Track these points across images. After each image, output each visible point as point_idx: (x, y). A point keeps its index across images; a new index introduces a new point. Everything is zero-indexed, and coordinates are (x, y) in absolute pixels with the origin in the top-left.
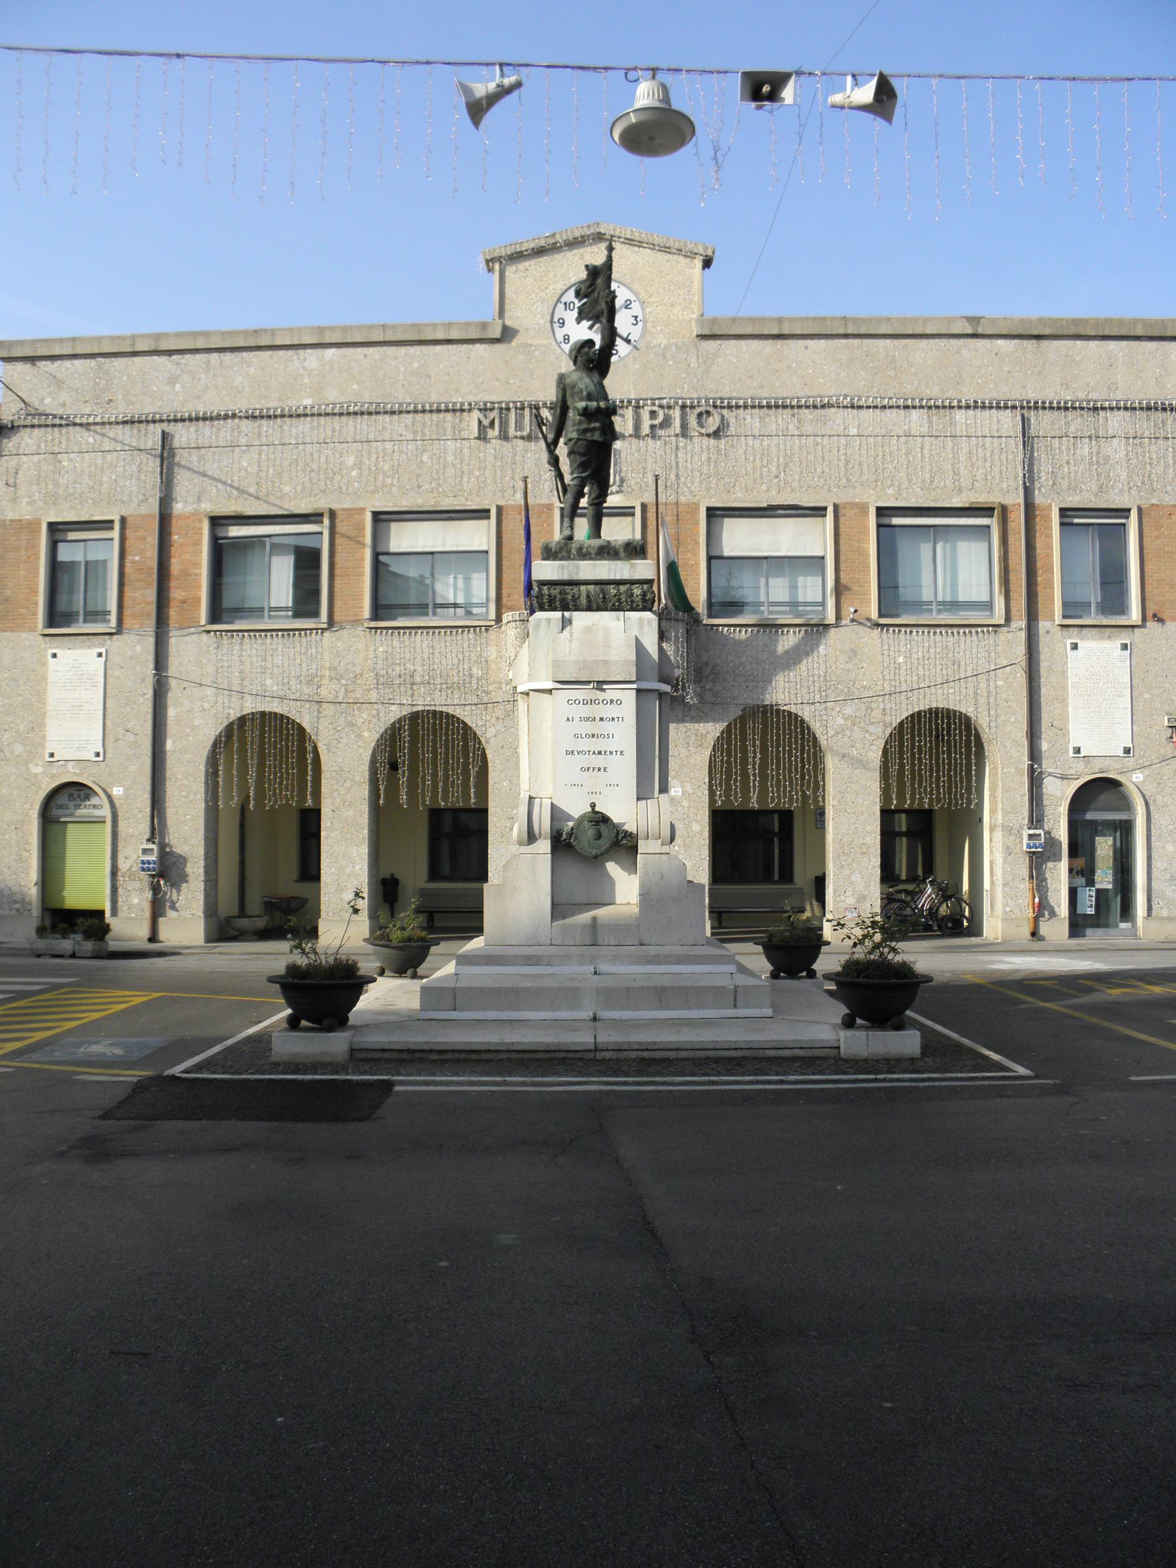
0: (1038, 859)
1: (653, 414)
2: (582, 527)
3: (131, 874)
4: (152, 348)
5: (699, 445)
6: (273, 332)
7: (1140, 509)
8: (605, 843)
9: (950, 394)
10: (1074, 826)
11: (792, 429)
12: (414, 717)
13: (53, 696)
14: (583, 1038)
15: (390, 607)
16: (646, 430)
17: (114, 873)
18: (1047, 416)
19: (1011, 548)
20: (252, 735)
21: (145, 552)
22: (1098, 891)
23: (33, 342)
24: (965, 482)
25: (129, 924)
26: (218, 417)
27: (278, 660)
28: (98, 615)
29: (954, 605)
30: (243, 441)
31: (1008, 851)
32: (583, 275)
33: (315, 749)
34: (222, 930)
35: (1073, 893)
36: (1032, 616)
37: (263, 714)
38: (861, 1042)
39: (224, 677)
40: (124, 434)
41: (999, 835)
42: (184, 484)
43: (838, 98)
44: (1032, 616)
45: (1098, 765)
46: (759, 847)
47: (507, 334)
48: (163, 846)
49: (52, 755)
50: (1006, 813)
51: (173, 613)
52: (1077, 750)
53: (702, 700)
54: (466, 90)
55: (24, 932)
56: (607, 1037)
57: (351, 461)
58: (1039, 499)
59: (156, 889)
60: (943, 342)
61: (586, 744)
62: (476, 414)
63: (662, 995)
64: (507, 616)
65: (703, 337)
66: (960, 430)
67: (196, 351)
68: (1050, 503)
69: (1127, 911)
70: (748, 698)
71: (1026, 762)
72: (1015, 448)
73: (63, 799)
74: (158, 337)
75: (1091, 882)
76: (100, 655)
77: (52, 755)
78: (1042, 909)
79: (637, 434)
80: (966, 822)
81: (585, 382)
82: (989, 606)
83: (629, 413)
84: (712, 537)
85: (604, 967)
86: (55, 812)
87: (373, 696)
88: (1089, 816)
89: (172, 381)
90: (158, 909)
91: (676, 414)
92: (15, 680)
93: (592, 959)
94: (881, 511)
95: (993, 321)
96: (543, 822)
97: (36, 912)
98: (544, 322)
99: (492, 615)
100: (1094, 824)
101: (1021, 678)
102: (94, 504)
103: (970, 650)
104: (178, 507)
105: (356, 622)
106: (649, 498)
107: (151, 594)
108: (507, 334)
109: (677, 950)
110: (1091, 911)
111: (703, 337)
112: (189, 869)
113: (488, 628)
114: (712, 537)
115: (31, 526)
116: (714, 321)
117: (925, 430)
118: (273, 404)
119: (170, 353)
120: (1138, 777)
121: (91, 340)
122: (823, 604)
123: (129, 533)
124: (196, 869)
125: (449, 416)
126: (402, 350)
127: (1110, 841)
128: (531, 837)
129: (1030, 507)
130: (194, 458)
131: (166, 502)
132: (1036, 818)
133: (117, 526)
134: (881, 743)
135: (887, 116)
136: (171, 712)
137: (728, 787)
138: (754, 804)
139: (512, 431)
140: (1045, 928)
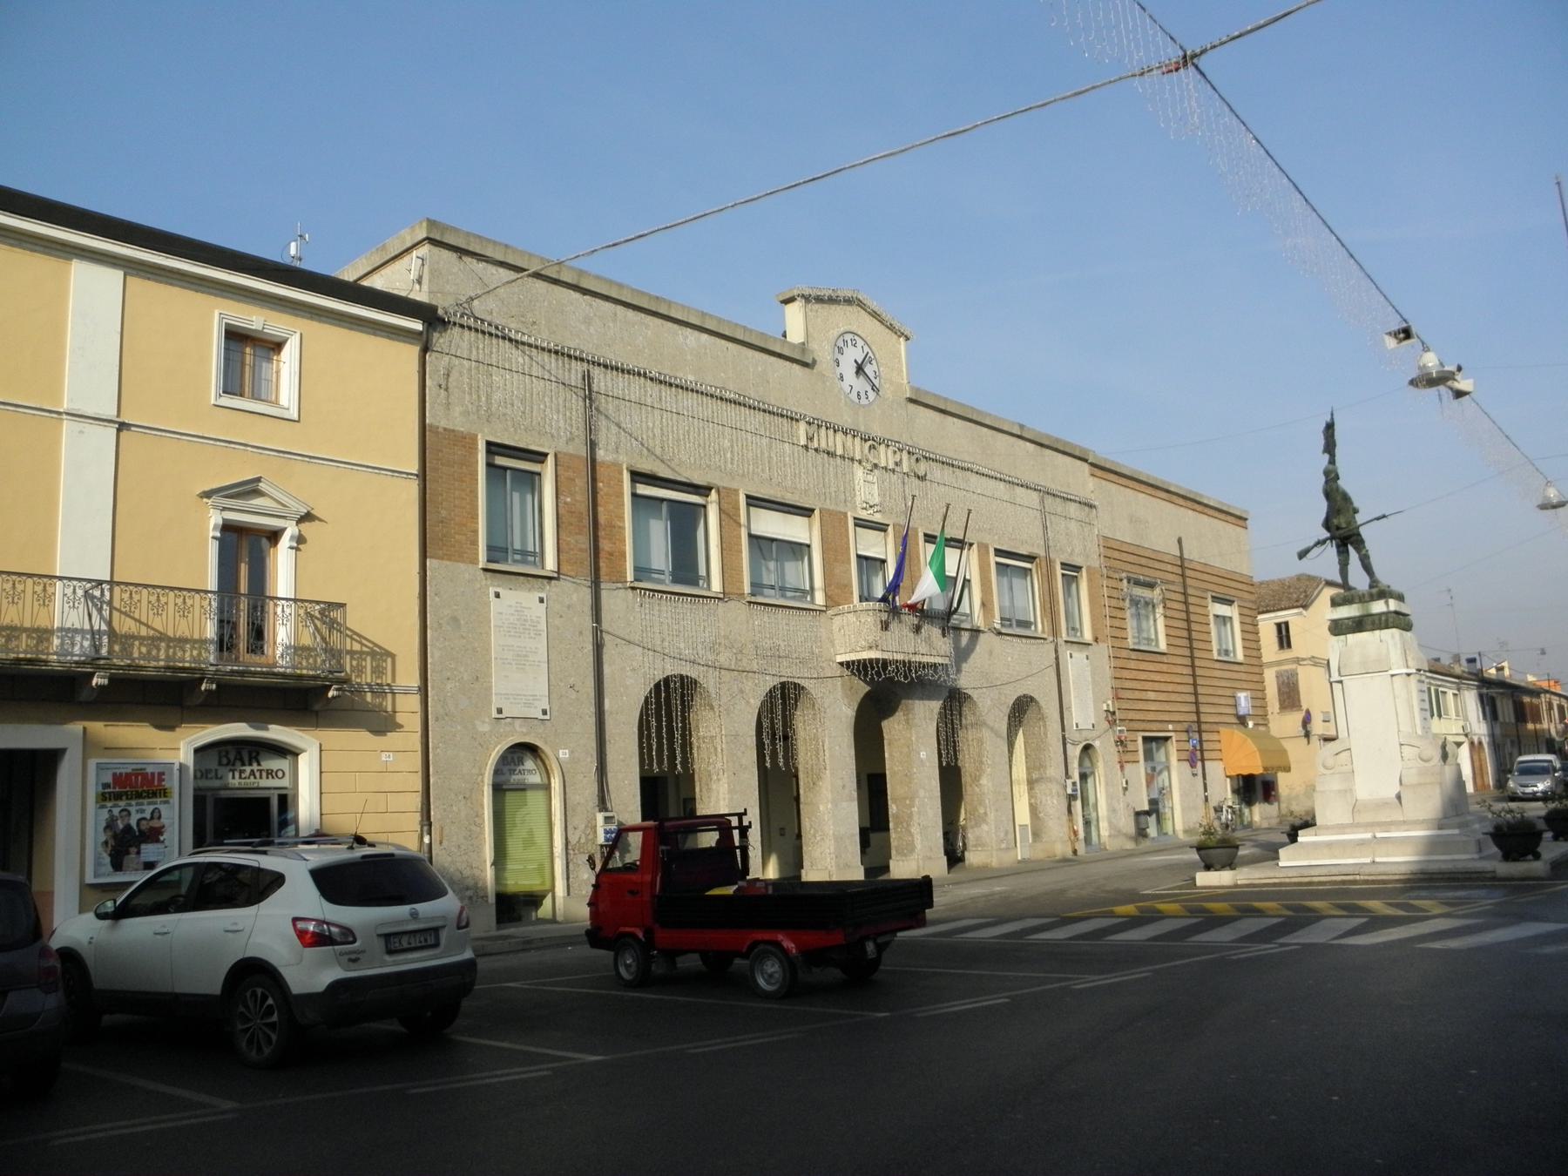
4: (574, 282)
6: (670, 303)
23: (468, 234)
40: (551, 362)
65: (911, 400)
76: (497, 595)
92: (455, 620)
97: (492, 899)
111: (911, 400)
116: (918, 390)
119: (585, 292)
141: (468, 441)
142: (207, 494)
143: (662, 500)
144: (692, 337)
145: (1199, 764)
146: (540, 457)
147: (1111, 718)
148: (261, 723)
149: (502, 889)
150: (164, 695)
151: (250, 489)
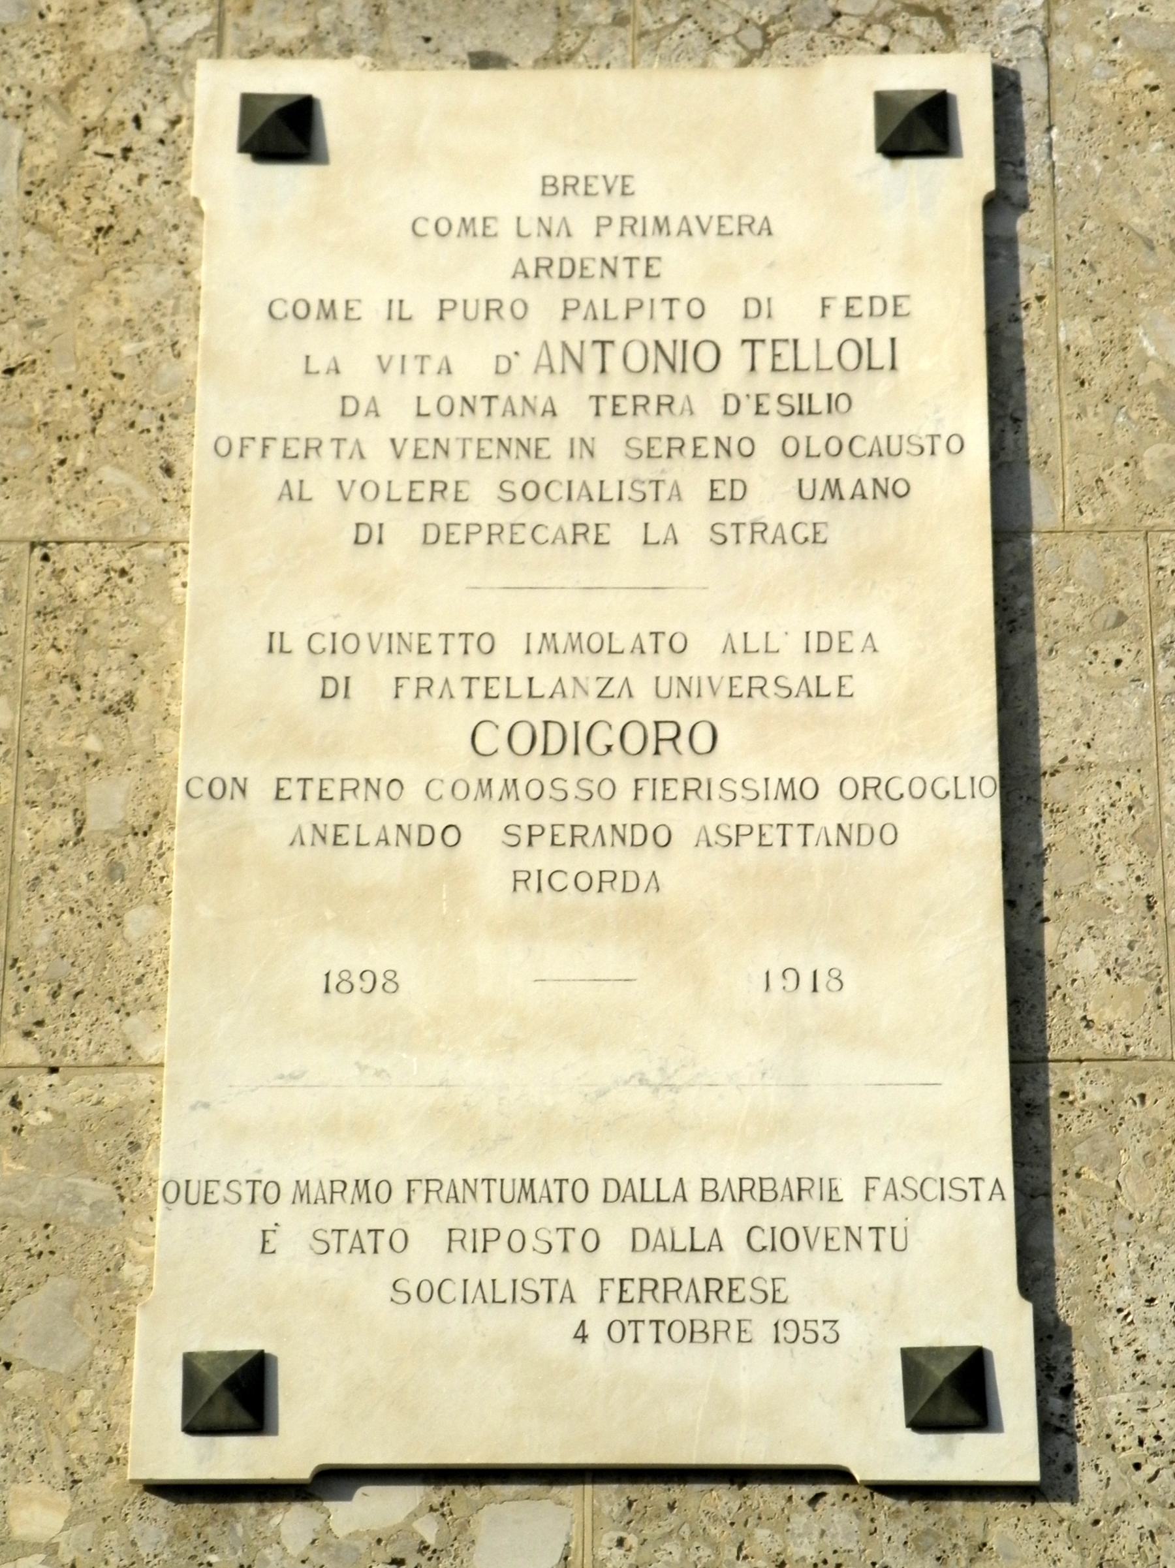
13: (250, 617)
49: (237, 1394)
77: (237, 1394)
102: (27, 702)
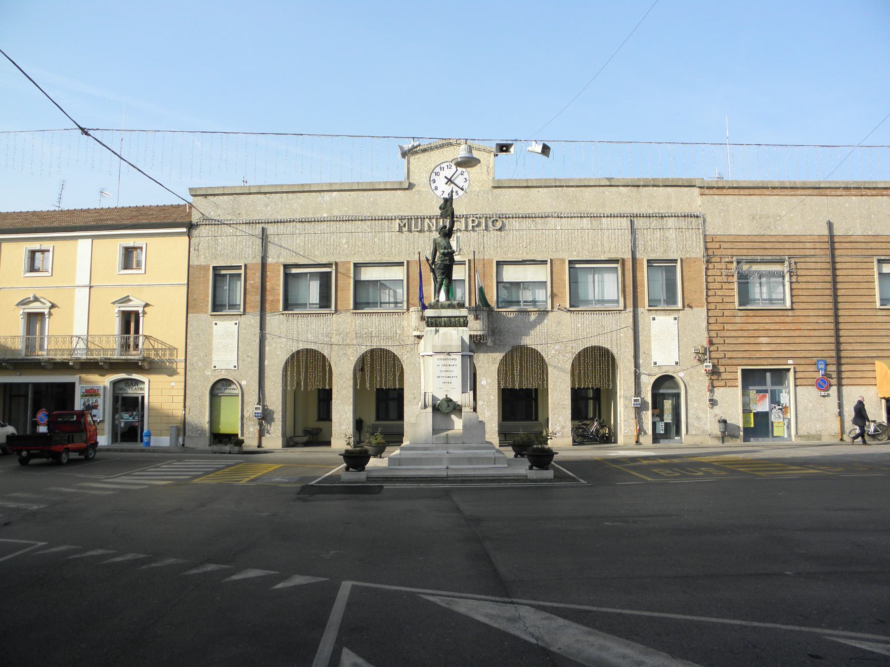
0: (639, 410)
1: (473, 221)
2: (442, 297)
3: (250, 419)
5: (493, 234)
6: (310, 185)
7: (681, 260)
8: (451, 408)
9: (600, 211)
10: (654, 396)
11: (533, 227)
12: (372, 351)
13: (215, 341)
14: (444, 473)
15: (360, 303)
16: (470, 228)
17: (242, 418)
18: (641, 220)
19: (626, 277)
20: (302, 358)
21: (255, 279)
22: (666, 424)
24: (607, 249)
25: (250, 441)
26: (287, 222)
27: (313, 326)
28: (233, 306)
29: (602, 301)
30: (298, 232)
31: (626, 407)
32: (443, 202)
33: (330, 364)
34: (289, 442)
35: (654, 424)
36: (635, 306)
37: (307, 350)
38: (536, 474)
39: (290, 334)
41: (622, 399)
42: (272, 251)
43: (530, 149)
44: (635, 306)
45: (664, 369)
46: (521, 404)
47: (411, 186)
48: (264, 406)
50: (625, 391)
51: (268, 306)
52: (655, 363)
53: (495, 343)
54: (401, 148)
55: (204, 443)
56: (450, 473)
57: (344, 241)
58: (638, 256)
59: (261, 425)
60: (597, 189)
61: (444, 374)
62: (398, 221)
63: (470, 460)
64: (411, 309)
66: (604, 226)
67: (277, 193)
68: (643, 257)
69: (678, 432)
70: (514, 343)
71: (633, 369)
72: (628, 233)
73: (219, 386)
74: (260, 187)
75: (662, 420)
78: (641, 431)
79: (466, 230)
80: (612, 394)
81: (443, 242)
82: (617, 301)
83: (463, 220)
84: (499, 273)
85: (450, 451)
86: (216, 391)
87: (355, 342)
88: (661, 391)
89: (266, 205)
90: (261, 433)
91: (483, 220)
92: (198, 335)
93: (446, 448)
94: (570, 262)
95: (618, 180)
96: (430, 401)
97: (208, 435)
98: (426, 181)
99: (405, 307)
100: (663, 394)
101: (631, 332)
103: (609, 321)
104: (270, 260)
105: (347, 310)
106: (471, 257)
107: (258, 298)
108: (411, 186)
109: (476, 445)
110: (662, 432)
112: (275, 416)
113: (403, 313)
114: (499, 273)
115: (206, 268)
116: (499, 181)
117: (589, 227)
118: (310, 216)
119: (265, 193)
120: (681, 374)
121: (231, 187)
122: (546, 302)
123: (248, 271)
124: (278, 416)
125: (386, 222)
126: (366, 193)
127: (670, 402)
128: (425, 407)
129: (634, 259)
130: (276, 239)
131: (264, 259)
132: (638, 392)
133: (243, 268)
134: (571, 361)
135: (548, 156)
136: (267, 349)
137: (506, 380)
138: (517, 387)
139: (413, 229)
140: (642, 439)
141: (491, 261)
142: (114, 303)
143: (306, 273)
144: (327, 195)
145: (834, 390)
146: (675, 261)
147: (702, 356)
148: (130, 374)
149: (216, 432)
150: (112, 366)
151: (126, 300)
